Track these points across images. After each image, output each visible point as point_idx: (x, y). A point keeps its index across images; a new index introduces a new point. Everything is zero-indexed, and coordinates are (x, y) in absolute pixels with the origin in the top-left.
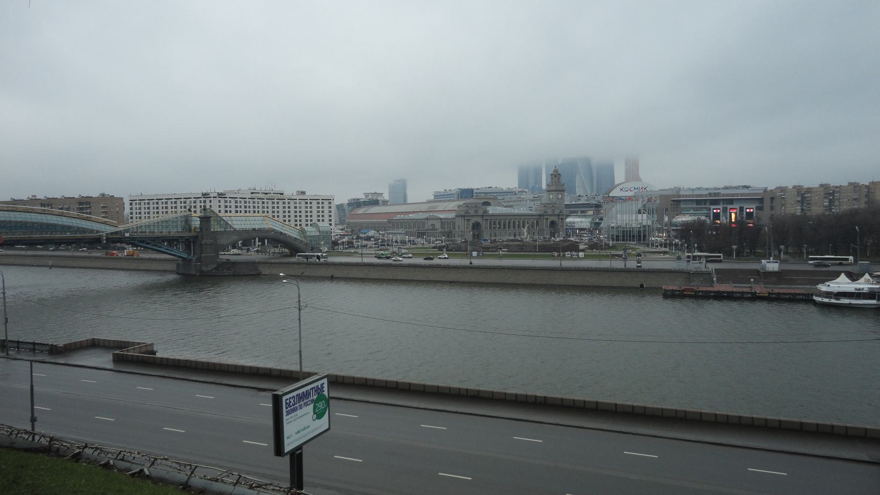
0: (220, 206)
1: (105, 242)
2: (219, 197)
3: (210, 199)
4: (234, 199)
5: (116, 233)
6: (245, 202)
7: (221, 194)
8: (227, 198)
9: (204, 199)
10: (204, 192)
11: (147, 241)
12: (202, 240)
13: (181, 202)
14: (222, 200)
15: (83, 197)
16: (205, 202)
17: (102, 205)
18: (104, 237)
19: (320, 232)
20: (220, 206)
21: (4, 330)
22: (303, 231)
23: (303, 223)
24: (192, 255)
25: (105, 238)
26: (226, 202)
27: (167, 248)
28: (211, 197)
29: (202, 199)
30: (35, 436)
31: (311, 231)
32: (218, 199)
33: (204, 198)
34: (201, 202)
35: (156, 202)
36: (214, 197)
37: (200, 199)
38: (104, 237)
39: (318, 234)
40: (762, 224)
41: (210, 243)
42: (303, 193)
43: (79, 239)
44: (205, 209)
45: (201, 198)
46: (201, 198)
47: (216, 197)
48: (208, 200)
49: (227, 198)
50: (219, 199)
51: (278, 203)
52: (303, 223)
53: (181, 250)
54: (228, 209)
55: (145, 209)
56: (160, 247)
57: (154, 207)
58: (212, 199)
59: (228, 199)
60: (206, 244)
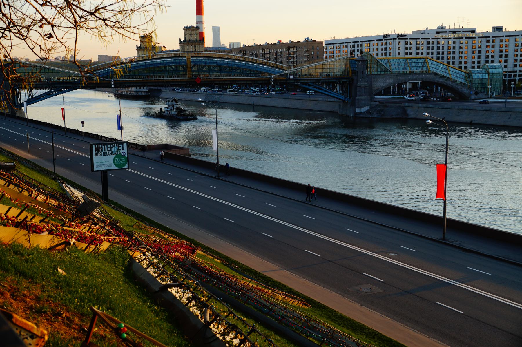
0: (399, 49)
1: (273, 83)
2: (399, 39)
3: (390, 41)
4: (426, 40)
5: (283, 75)
6: (428, 43)
7: (402, 35)
8: (407, 39)
9: (385, 41)
10: (386, 33)
11: (309, 83)
12: (357, 83)
13: (351, 46)
14: (402, 42)
15: (292, 42)
16: (386, 44)
17: (305, 50)
18: (272, 79)
19: (489, 75)
20: (399, 49)
21: (448, 158)
22: (469, 75)
23: (469, 65)
24: (349, 97)
25: (273, 80)
26: (406, 43)
27: (326, 90)
28: (391, 39)
29: (384, 42)
30: (442, 238)
31: (478, 75)
32: (398, 41)
33: (385, 40)
34: (382, 45)
35: (360, 44)
36: (394, 39)
37: (382, 41)
38: (272, 79)
39: (487, 77)
40: (391, 79)
41: (364, 86)
42: (500, 29)
43: (254, 81)
44: (361, 52)
45: (382, 40)
46: (382, 40)
47: (396, 39)
48: (388, 42)
49: (407, 39)
50: (399, 40)
51: (454, 43)
52: (469, 65)
53: (338, 92)
54: (408, 51)
55: (382, 50)
56: (321, 89)
57: (382, 48)
58: (392, 41)
59: (409, 41)
60: (360, 87)
